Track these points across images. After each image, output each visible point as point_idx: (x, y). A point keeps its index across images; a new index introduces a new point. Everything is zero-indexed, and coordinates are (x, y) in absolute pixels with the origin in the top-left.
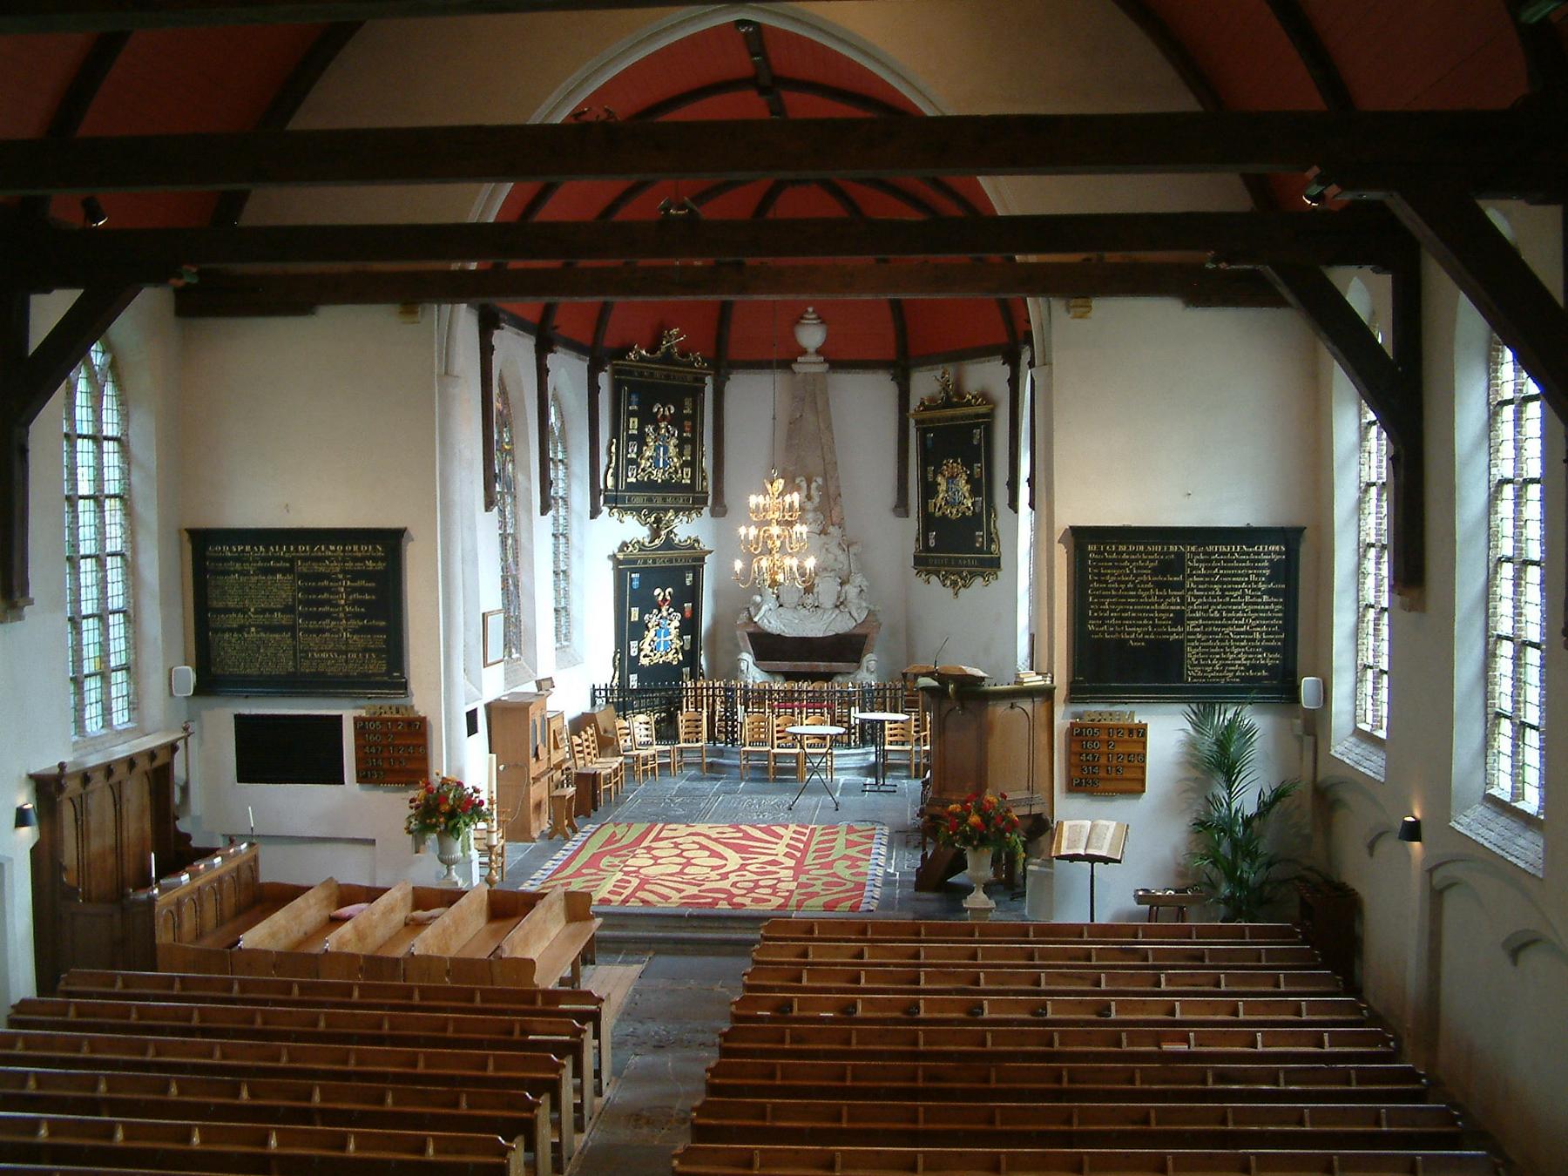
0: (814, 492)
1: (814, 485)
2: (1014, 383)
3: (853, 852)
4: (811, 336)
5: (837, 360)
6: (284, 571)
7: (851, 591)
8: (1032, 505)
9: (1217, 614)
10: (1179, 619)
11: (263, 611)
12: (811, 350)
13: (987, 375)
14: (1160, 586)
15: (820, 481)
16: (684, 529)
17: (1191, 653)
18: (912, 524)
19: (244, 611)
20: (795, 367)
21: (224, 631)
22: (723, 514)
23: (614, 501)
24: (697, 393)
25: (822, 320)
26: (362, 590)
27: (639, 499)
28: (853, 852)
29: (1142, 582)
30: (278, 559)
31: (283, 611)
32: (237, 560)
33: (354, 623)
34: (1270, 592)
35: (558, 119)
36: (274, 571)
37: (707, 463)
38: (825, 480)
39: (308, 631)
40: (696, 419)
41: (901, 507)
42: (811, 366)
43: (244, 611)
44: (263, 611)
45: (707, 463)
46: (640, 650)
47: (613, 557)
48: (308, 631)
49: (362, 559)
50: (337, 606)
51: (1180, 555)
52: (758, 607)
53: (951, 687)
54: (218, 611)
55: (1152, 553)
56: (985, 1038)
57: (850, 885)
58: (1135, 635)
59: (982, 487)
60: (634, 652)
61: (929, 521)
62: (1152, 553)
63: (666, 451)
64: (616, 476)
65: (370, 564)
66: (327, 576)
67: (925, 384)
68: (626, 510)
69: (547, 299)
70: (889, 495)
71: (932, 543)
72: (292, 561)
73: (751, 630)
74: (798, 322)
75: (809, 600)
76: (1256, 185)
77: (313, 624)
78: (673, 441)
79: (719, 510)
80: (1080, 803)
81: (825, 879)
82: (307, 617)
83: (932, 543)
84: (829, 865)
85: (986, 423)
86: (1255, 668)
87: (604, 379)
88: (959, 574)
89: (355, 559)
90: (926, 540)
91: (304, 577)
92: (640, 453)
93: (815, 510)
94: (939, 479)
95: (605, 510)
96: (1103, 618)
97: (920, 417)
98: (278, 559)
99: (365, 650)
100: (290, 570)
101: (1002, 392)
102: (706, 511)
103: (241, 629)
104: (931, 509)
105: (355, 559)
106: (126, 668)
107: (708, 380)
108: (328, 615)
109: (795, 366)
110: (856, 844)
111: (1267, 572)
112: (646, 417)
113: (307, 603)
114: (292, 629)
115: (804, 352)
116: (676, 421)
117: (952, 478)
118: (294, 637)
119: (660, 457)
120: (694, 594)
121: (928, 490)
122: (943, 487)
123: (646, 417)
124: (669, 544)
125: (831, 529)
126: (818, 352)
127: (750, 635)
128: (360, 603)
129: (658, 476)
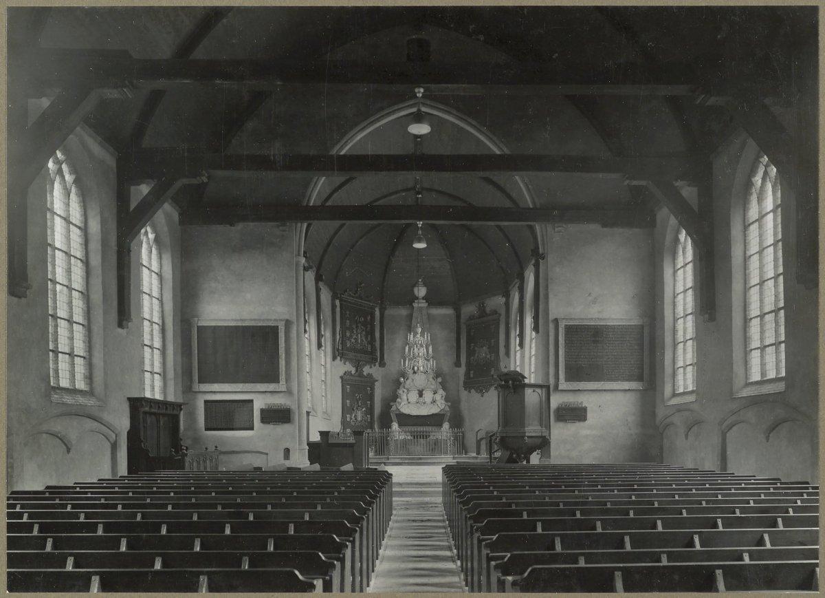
4: (421, 291)
5: (431, 300)
7: (438, 397)
8: (536, 328)
13: (498, 301)
16: (367, 370)
18: (462, 370)
23: (342, 356)
25: (425, 285)
27: (351, 355)
37: (377, 335)
41: (458, 364)
45: (377, 335)
46: (351, 419)
47: (341, 377)
53: (510, 382)
56: (762, 537)
60: (348, 419)
64: (342, 343)
67: (469, 309)
69: (309, 222)
79: (382, 364)
83: (472, 376)
87: (337, 302)
92: (351, 336)
95: (339, 358)
115: (417, 298)
121: (470, 353)
124: (361, 375)
126: (423, 298)
127: (396, 415)
129: (359, 347)
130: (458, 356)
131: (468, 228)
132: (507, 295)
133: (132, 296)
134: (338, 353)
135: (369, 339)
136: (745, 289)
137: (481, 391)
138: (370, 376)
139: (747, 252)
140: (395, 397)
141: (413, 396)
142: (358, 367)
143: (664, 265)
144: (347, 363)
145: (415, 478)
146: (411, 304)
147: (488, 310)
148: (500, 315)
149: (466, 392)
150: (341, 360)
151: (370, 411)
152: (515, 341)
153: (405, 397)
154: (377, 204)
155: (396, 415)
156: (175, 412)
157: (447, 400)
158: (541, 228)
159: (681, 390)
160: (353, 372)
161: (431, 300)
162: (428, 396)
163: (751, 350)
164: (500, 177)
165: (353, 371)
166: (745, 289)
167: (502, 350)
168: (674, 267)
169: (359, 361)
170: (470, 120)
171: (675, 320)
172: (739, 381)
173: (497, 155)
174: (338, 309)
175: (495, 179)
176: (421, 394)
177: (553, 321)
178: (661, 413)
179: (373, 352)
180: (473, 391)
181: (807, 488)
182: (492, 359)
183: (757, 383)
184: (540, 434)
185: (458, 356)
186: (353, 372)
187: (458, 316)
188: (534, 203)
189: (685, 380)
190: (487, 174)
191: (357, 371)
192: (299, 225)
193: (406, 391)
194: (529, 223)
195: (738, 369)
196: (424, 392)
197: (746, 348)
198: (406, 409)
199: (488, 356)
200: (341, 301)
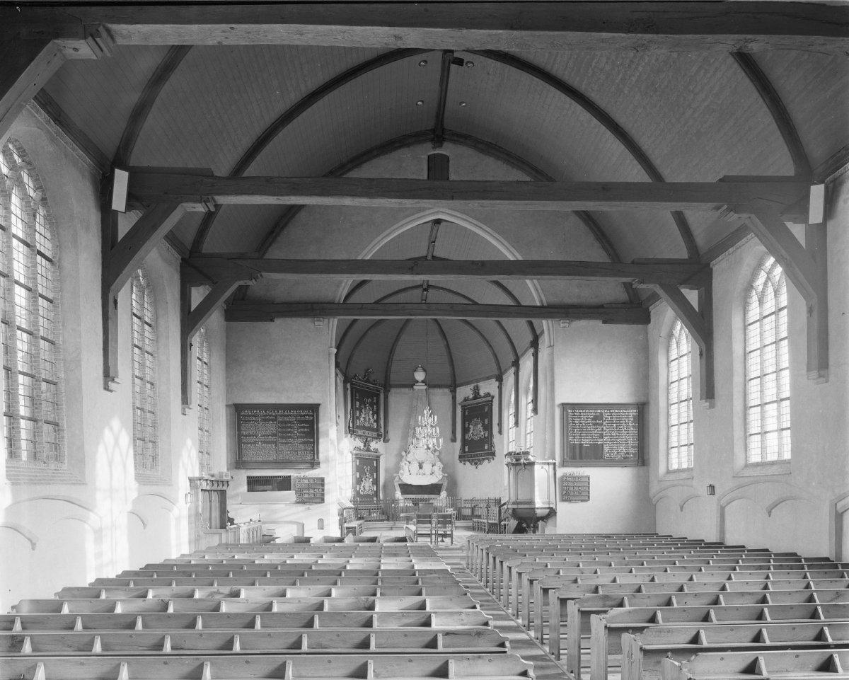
2: (500, 388)
4: (420, 376)
5: (430, 384)
6: (273, 420)
7: (436, 468)
9: (614, 434)
10: (601, 436)
11: (264, 436)
14: (594, 424)
17: (606, 449)
18: (458, 444)
19: (256, 436)
20: (415, 387)
21: (247, 444)
22: (388, 441)
24: (378, 396)
25: (425, 370)
26: (304, 427)
27: (360, 432)
30: (270, 416)
31: (272, 436)
32: (254, 416)
33: (301, 440)
34: (633, 427)
35: (368, 258)
36: (269, 420)
37: (382, 422)
39: (282, 443)
40: (378, 403)
41: (454, 440)
42: (420, 387)
43: (256, 436)
44: (264, 436)
45: (382, 422)
48: (282, 443)
49: (304, 416)
50: (294, 433)
51: (601, 413)
52: (403, 474)
54: (246, 436)
58: (586, 442)
59: (488, 428)
63: (369, 416)
64: (353, 422)
65: (307, 417)
66: (290, 422)
68: (357, 436)
71: (467, 450)
72: (276, 416)
74: (415, 371)
75: (421, 471)
76: (627, 286)
77: (284, 441)
78: (371, 412)
79: (386, 441)
80: (566, 504)
82: (282, 438)
83: (467, 450)
85: (490, 404)
86: (628, 453)
87: (349, 385)
88: (478, 460)
89: (301, 416)
90: (464, 448)
91: (282, 422)
92: (360, 415)
94: (471, 426)
96: (574, 436)
97: (463, 404)
98: (270, 416)
99: (305, 450)
100: (275, 420)
101: (495, 392)
102: (382, 440)
103: (255, 442)
104: (466, 438)
105: (301, 416)
106: (266, 411)
107: (382, 391)
108: (290, 437)
111: (632, 419)
112: (363, 403)
113: (282, 433)
114: (275, 442)
115: (418, 382)
116: (371, 405)
117: (476, 425)
118: (276, 446)
119: (367, 417)
120: (377, 470)
123: (363, 403)
126: (423, 382)
127: (399, 485)
128: (304, 433)
129: (367, 425)
130: (454, 432)
131: (466, 322)
132: (500, 379)
133: (651, 435)
134: (351, 431)
135: (375, 417)
136: (745, 381)
137: (476, 464)
138: (376, 451)
139: (747, 349)
140: (398, 468)
141: (415, 466)
142: (366, 443)
143: (659, 357)
144: (357, 439)
145: (216, 517)
146: (412, 387)
147: (482, 393)
148: (493, 397)
149: (462, 464)
150: (351, 437)
151: (376, 482)
152: (509, 420)
153: (406, 468)
154: (391, 300)
155: (399, 485)
156: (224, 488)
157: (444, 471)
158: (548, 324)
159: (675, 467)
160: (362, 448)
161: (430, 384)
162: (427, 467)
163: (751, 435)
164: (510, 282)
165: (362, 445)
166: (745, 381)
167: (495, 429)
168: (668, 359)
169: (367, 437)
170: (485, 227)
171: (669, 405)
172: (740, 462)
173: (510, 261)
174: (349, 392)
175: (504, 283)
176: (421, 467)
177: (559, 405)
178: (654, 488)
179: (377, 430)
180: (467, 463)
181: (721, 547)
182: (486, 436)
183: (757, 465)
184: (548, 506)
185: (454, 432)
186: (362, 448)
187: (454, 398)
188: (541, 301)
189: (679, 458)
190: (495, 278)
191: (365, 446)
192: (332, 320)
193: (408, 463)
194: (530, 319)
195: (738, 448)
196: (424, 465)
197: (746, 433)
198: (409, 480)
199: (482, 433)
200: (351, 384)
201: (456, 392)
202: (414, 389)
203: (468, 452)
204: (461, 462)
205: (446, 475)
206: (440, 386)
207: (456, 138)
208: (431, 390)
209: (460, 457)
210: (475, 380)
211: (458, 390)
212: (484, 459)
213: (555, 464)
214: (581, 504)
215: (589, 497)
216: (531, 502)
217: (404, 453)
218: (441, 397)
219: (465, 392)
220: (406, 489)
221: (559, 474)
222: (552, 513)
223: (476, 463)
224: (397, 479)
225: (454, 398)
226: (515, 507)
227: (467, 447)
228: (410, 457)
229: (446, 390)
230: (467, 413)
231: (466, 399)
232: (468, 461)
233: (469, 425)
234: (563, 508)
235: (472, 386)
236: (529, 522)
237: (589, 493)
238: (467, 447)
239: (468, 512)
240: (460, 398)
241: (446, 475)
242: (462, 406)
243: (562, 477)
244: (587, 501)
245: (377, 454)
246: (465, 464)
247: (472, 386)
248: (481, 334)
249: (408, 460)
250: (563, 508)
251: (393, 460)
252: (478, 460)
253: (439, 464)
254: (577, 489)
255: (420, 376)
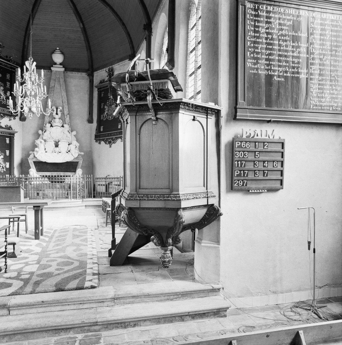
0: (59, 112)
1: (59, 110)
3: (77, 241)
7: (72, 147)
12: (58, 63)
15: (61, 108)
18: (95, 124)
20: (52, 69)
25: (62, 53)
28: (77, 241)
29: (282, 35)
38: (63, 108)
41: (90, 121)
42: (58, 69)
55: (289, 15)
57: (77, 264)
61: (100, 122)
62: (289, 15)
70: (85, 115)
71: (102, 130)
73: (35, 160)
75: (57, 149)
81: (60, 260)
83: (102, 130)
84: (63, 250)
88: (112, 139)
93: (59, 119)
94: (106, 107)
104: (102, 118)
109: (52, 68)
110: (78, 236)
115: (56, 64)
120: (10, 147)
121: (101, 111)
122: (107, 110)
125: (65, 125)
126: (61, 64)
127: (34, 162)
137: (110, 143)
149: (97, 144)
155: (34, 162)
161: (67, 67)
162: (63, 146)
176: (57, 146)
180: (102, 142)
184: (204, 202)
187: (91, 82)
193: (43, 141)
201: (93, 76)
202: (52, 71)
203: (102, 132)
204: (96, 141)
205: (82, 153)
206: (78, 70)
207: (175, 299)
208: (70, 74)
209: (96, 136)
210: (108, 63)
211: (96, 74)
212: (117, 138)
213: (217, 113)
214: (266, 198)
215: (282, 181)
216: (171, 191)
217: (40, 132)
218: (79, 82)
219: (101, 75)
220: (41, 166)
221: (226, 137)
222: (212, 214)
223: (110, 142)
224: (31, 156)
225: (91, 82)
226: (134, 204)
227: (102, 127)
228: (46, 136)
229: (84, 74)
230: (102, 95)
231: (102, 82)
232: (103, 140)
233: (104, 106)
234: (231, 205)
235: (107, 69)
236: (164, 235)
237: (282, 175)
238: (102, 127)
239: (102, 189)
240: (96, 81)
241: (82, 153)
242: (98, 89)
243: (232, 145)
244: (276, 190)
245: (10, 131)
246: (100, 143)
247: (107, 69)
248: (123, 24)
249: (44, 138)
250: (231, 205)
251: (30, 138)
252: (112, 139)
253: (75, 143)
254: (260, 166)
255: (58, 58)
